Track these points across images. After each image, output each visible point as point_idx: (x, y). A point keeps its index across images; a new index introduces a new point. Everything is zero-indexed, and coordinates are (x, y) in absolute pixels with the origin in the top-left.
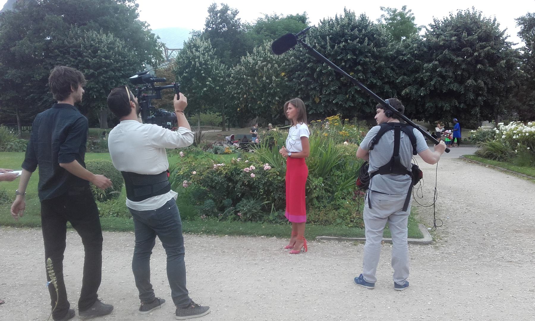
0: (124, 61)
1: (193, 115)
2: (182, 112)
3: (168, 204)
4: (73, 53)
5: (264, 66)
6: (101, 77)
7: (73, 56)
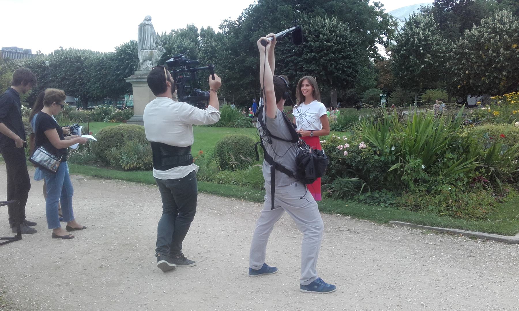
0: (344, 43)
1: (424, 94)
2: (216, 91)
3: (191, 175)
5: (490, 38)
6: (322, 60)
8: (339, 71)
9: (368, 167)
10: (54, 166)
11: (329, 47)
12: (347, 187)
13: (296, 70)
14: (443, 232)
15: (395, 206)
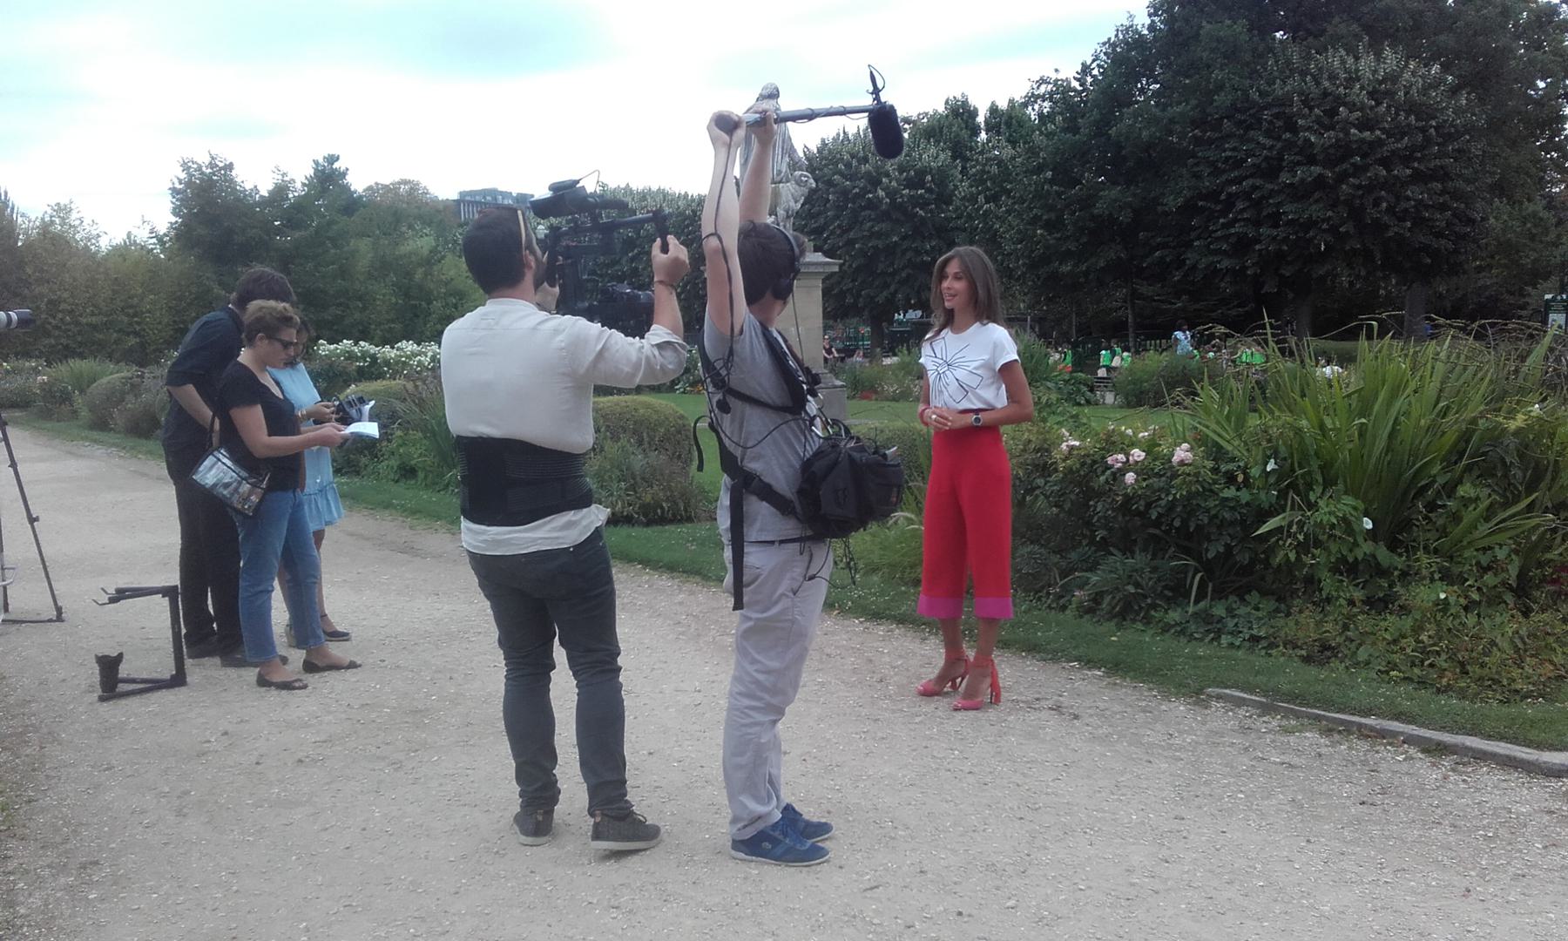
0: (1423, 130)
4: (1271, 122)
7: (1268, 134)
8: (1405, 221)
9: (1200, 522)
10: (247, 499)
11: (1371, 144)
12: (1137, 585)
13: (1257, 224)
14: (1348, 729)
15: (1265, 645)
